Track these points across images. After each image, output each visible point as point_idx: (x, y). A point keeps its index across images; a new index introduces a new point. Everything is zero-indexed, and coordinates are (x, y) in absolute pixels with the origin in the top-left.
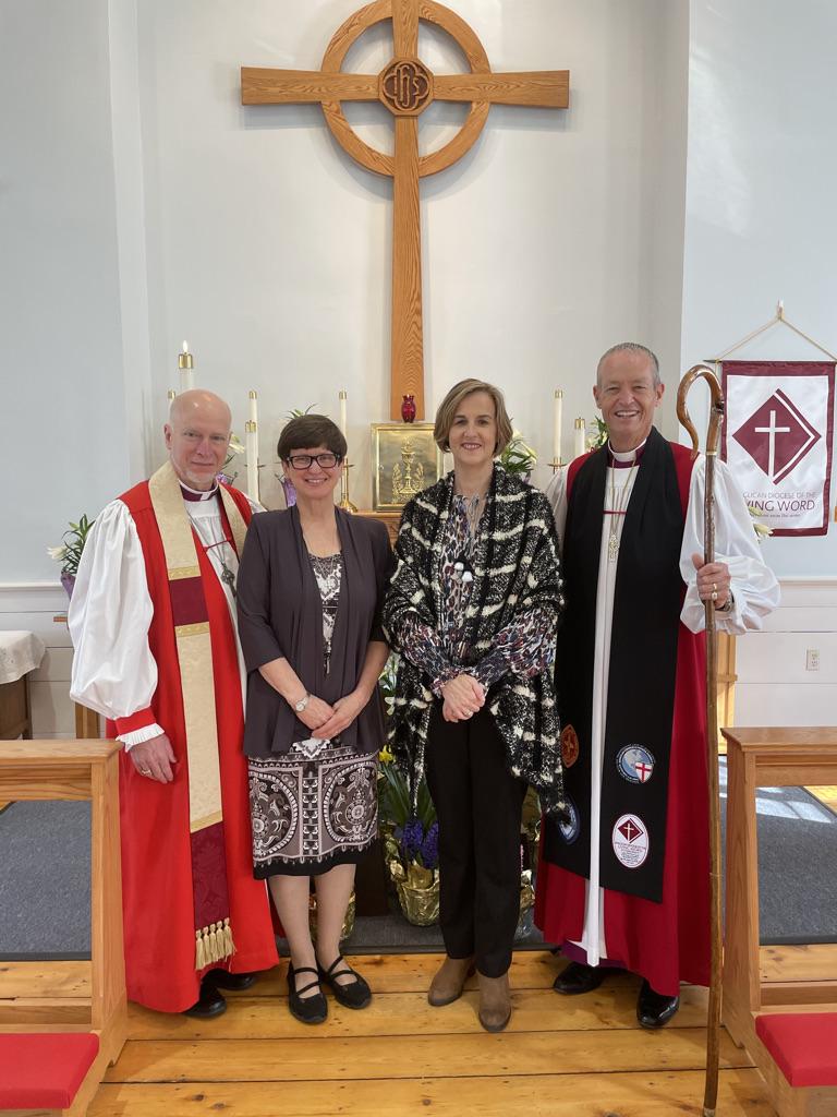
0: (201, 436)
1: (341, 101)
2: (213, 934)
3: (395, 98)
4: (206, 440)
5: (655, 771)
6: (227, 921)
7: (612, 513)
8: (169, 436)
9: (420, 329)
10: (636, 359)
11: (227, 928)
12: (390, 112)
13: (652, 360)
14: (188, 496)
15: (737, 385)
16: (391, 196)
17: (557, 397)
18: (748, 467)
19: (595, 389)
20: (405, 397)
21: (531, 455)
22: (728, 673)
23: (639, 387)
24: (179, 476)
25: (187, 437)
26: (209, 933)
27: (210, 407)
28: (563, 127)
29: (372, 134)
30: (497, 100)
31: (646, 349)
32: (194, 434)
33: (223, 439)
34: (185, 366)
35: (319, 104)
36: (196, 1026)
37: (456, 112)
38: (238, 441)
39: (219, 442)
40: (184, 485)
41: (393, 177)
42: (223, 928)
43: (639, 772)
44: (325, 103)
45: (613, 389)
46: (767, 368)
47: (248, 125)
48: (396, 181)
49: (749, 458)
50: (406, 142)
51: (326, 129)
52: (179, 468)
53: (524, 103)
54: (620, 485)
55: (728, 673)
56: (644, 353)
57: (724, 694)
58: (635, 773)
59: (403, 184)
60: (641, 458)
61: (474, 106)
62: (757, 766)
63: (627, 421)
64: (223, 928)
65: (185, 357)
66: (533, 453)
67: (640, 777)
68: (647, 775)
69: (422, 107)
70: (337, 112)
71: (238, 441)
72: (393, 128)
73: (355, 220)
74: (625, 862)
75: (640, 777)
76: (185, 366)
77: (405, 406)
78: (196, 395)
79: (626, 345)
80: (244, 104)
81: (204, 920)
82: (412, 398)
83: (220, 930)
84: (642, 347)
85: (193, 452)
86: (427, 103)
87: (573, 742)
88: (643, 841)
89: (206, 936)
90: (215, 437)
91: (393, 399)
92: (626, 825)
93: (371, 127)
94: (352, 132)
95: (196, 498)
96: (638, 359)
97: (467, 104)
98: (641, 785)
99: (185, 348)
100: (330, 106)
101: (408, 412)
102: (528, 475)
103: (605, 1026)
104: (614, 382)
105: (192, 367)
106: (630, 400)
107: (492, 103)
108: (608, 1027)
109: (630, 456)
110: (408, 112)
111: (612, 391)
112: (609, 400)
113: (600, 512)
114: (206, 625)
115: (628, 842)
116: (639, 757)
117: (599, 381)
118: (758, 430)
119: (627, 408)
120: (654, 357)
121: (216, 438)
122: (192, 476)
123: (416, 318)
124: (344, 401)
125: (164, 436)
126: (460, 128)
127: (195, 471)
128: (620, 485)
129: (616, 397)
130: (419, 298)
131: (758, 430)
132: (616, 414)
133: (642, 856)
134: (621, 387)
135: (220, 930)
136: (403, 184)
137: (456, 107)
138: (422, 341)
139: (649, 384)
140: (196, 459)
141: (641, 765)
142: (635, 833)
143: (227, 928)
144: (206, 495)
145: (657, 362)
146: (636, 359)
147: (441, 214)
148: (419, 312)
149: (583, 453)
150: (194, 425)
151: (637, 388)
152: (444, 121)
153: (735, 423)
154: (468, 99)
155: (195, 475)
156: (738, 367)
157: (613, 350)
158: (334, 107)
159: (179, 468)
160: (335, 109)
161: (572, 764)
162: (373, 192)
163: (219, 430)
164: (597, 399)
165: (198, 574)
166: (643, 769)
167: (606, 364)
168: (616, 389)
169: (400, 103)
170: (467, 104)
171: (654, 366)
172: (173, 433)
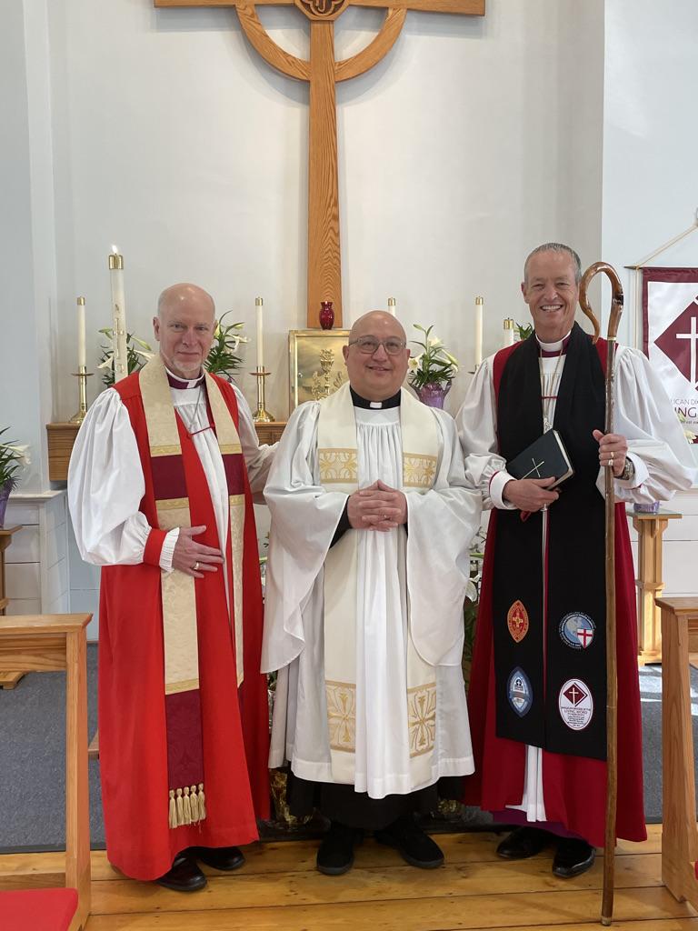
0: (185, 327)
1: (256, 5)
2: (186, 797)
3: (311, 3)
4: (191, 330)
5: (595, 636)
6: (201, 786)
7: (550, 398)
8: (157, 328)
9: (337, 235)
10: (560, 257)
11: (201, 793)
12: (307, 17)
13: (574, 259)
14: (174, 384)
15: (658, 290)
16: (307, 101)
17: (477, 303)
18: (670, 373)
19: (523, 286)
20: (323, 304)
21: (453, 363)
22: (655, 581)
23: (562, 284)
24: (166, 364)
25: (174, 328)
26: (183, 795)
27: (194, 298)
28: (479, 34)
29: (286, 38)
30: (414, 7)
31: (568, 248)
32: (180, 326)
33: (207, 329)
34: (116, 267)
35: (232, 8)
36: (170, 898)
37: (371, 18)
38: (150, 349)
39: (203, 332)
40: (170, 373)
41: (309, 82)
42: (197, 792)
43: (581, 638)
44: (240, 6)
45: (538, 285)
46: (687, 274)
47: (160, 27)
48: (312, 83)
49: (671, 365)
50: (322, 48)
51: (240, 32)
52: (166, 356)
53: (440, 10)
54: (551, 370)
55: (655, 581)
56: (565, 252)
57: (657, 644)
58: (577, 640)
59: (318, 89)
60: (568, 348)
61: (390, 12)
62: (689, 630)
63: (552, 315)
64: (197, 792)
65: (115, 258)
66: (454, 360)
67: (582, 643)
68: (589, 640)
69: (340, 11)
70: (252, 15)
71: (150, 349)
72: (308, 33)
73: (270, 124)
74: (571, 726)
75: (582, 643)
76: (116, 267)
77: (322, 312)
78: (182, 289)
79: (550, 245)
80: (156, 7)
81: (179, 779)
82: (331, 303)
83: (194, 794)
84: (565, 247)
85: (179, 342)
86: (342, 8)
87: (521, 617)
88: (587, 703)
89: (179, 798)
90: (199, 328)
91: (310, 308)
92: (571, 689)
93: (286, 31)
94: (267, 36)
95: (183, 386)
96: (561, 258)
97: (383, 10)
98: (584, 650)
99: (115, 250)
100: (244, 8)
101: (326, 318)
102: (449, 383)
103: (552, 889)
104: (538, 280)
105: (122, 269)
106: (554, 296)
107: (408, 9)
108: (555, 889)
109: (557, 346)
110: (324, 17)
111: (538, 288)
112: (534, 297)
113: (538, 399)
114: (186, 501)
115: (573, 706)
116: (580, 623)
117: (526, 279)
118: (679, 336)
119: (551, 303)
120: (576, 256)
121: (201, 329)
122: (179, 366)
123: (332, 223)
124: (260, 308)
125: (152, 328)
126: (377, 34)
127: (182, 360)
128: (551, 370)
129: (542, 293)
130: (336, 204)
131: (679, 336)
132: (541, 308)
133: (587, 717)
134: (549, 282)
135: (194, 794)
136: (318, 89)
137: (373, 12)
138: (339, 247)
139: (571, 280)
140: (181, 348)
141: (582, 631)
142: (580, 696)
143: (201, 793)
144: (192, 383)
145: (578, 260)
146: (560, 257)
147: (359, 119)
148: (336, 218)
149: (512, 343)
150: (180, 317)
151: (560, 284)
152: (360, 27)
153: (656, 332)
154: (384, 5)
155: (182, 364)
156: (659, 274)
157: (538, 250)
158: (249, 11)
159: (166, 356)
160: (251, 12)
161: (522, 638)
162: (288, 97)
163: (202, 320)
164: (525, 294)
165: (180, 452)
166: (585, 635)
167: (532, 263)
168: (541, 285)
169: (316, 8)
170: (383, 10)
171: (576, 264)
172: (160, 325)
